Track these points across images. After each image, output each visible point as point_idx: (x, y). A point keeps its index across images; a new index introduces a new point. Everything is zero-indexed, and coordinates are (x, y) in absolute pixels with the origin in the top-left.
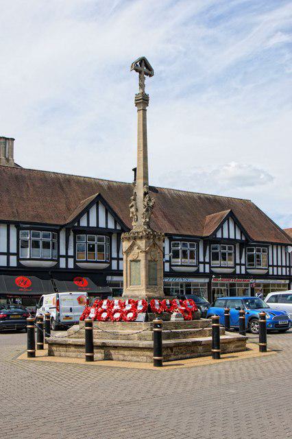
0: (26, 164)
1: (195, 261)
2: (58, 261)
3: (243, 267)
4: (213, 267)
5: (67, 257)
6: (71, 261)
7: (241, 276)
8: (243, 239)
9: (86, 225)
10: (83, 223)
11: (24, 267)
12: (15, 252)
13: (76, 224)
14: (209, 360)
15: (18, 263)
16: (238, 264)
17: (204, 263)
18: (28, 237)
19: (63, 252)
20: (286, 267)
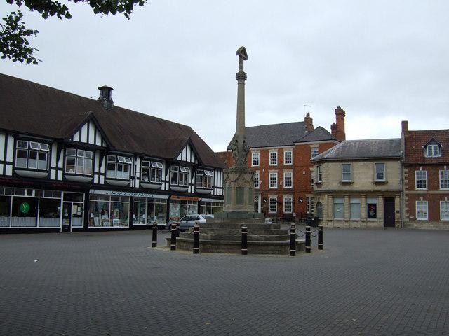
0: (115, 104)
4: (142, 182)
7: (191, 194)
8: (104, 145)
11: (199, 194)
12: (62, 167)
14: (287, 257)
15: (14, 172)
16: (96, 173)
17: (57, 169)
20: (223, 188)
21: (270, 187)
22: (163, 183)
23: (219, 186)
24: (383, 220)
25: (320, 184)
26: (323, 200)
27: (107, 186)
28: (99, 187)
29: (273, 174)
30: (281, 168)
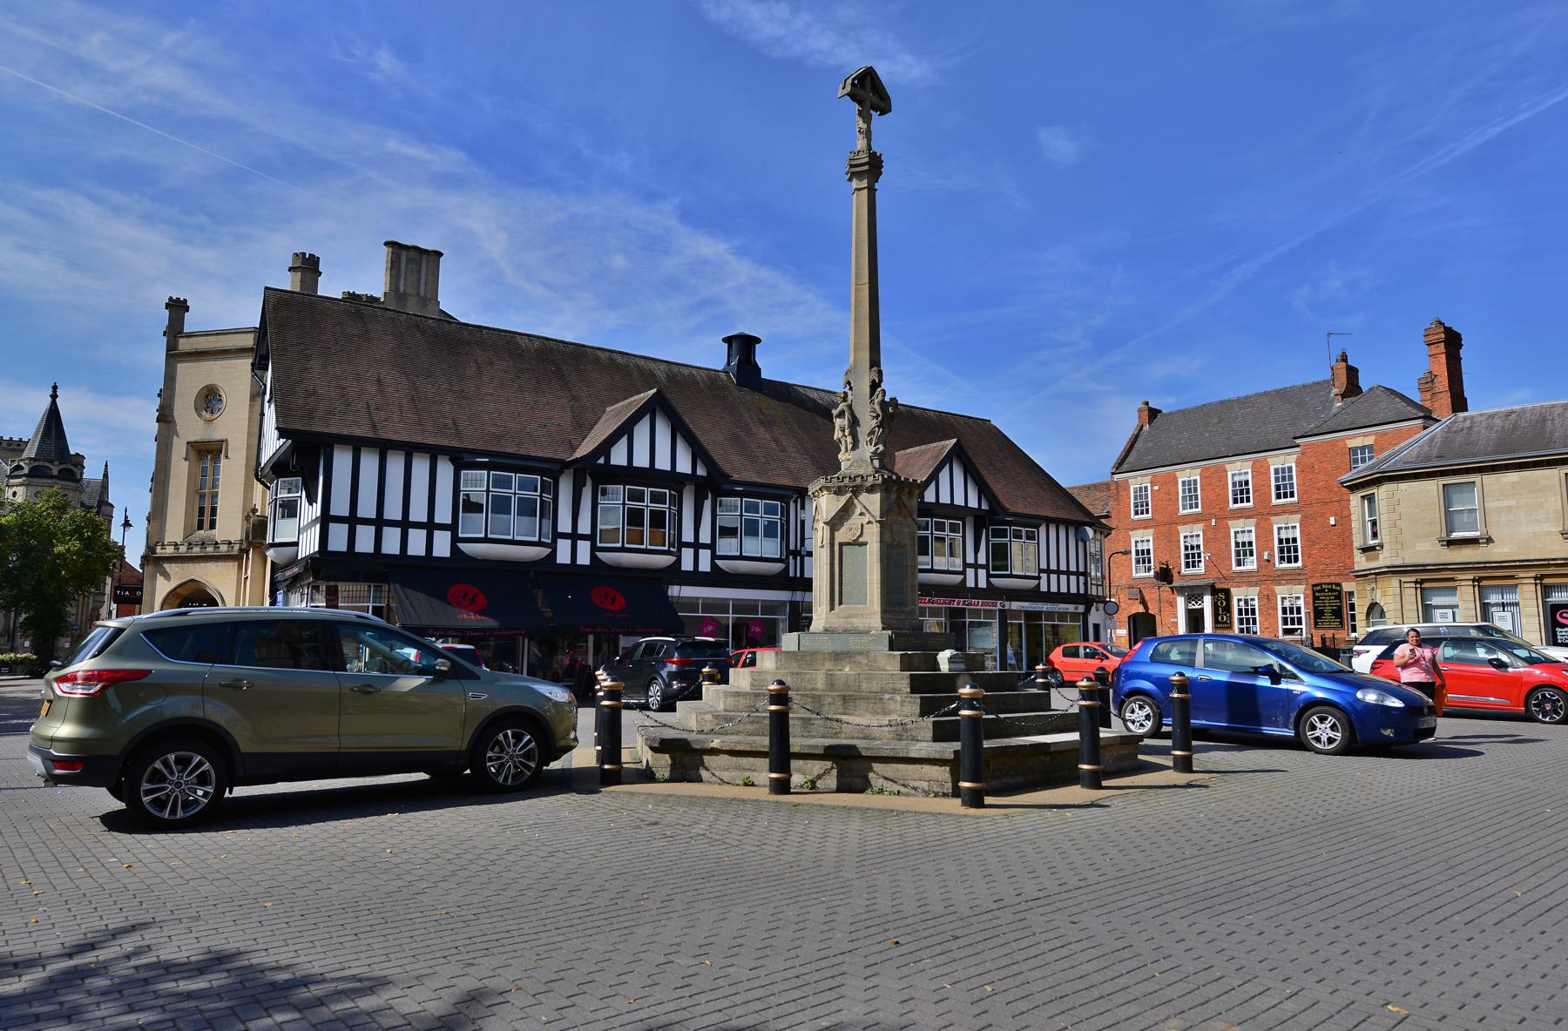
1: (958, 561)
2: (553, 546)
3: (982, 573)
5: (574, 537)
6: (584, 548)
7: (977, 593)
8: (985, 506)
9: (934, 501)
10: (618, 457)
13: (601, 461)
16: (970, 566)
18: (478, 483)
19: (565, 526)
20: (1077, 574)
21: (1235, 568)
22: (1044, 576)
23: (1073, 568)
24: (791, 722)
25: (1372, 548)
26: (1384, 594)
27: (717, 577)
28: (696, 578)
29: (1243, 530)
30: (1263, 514)
